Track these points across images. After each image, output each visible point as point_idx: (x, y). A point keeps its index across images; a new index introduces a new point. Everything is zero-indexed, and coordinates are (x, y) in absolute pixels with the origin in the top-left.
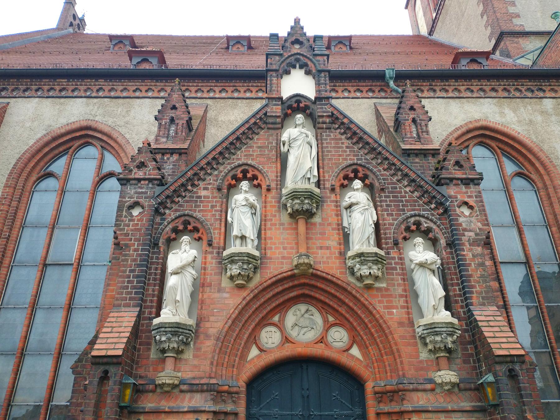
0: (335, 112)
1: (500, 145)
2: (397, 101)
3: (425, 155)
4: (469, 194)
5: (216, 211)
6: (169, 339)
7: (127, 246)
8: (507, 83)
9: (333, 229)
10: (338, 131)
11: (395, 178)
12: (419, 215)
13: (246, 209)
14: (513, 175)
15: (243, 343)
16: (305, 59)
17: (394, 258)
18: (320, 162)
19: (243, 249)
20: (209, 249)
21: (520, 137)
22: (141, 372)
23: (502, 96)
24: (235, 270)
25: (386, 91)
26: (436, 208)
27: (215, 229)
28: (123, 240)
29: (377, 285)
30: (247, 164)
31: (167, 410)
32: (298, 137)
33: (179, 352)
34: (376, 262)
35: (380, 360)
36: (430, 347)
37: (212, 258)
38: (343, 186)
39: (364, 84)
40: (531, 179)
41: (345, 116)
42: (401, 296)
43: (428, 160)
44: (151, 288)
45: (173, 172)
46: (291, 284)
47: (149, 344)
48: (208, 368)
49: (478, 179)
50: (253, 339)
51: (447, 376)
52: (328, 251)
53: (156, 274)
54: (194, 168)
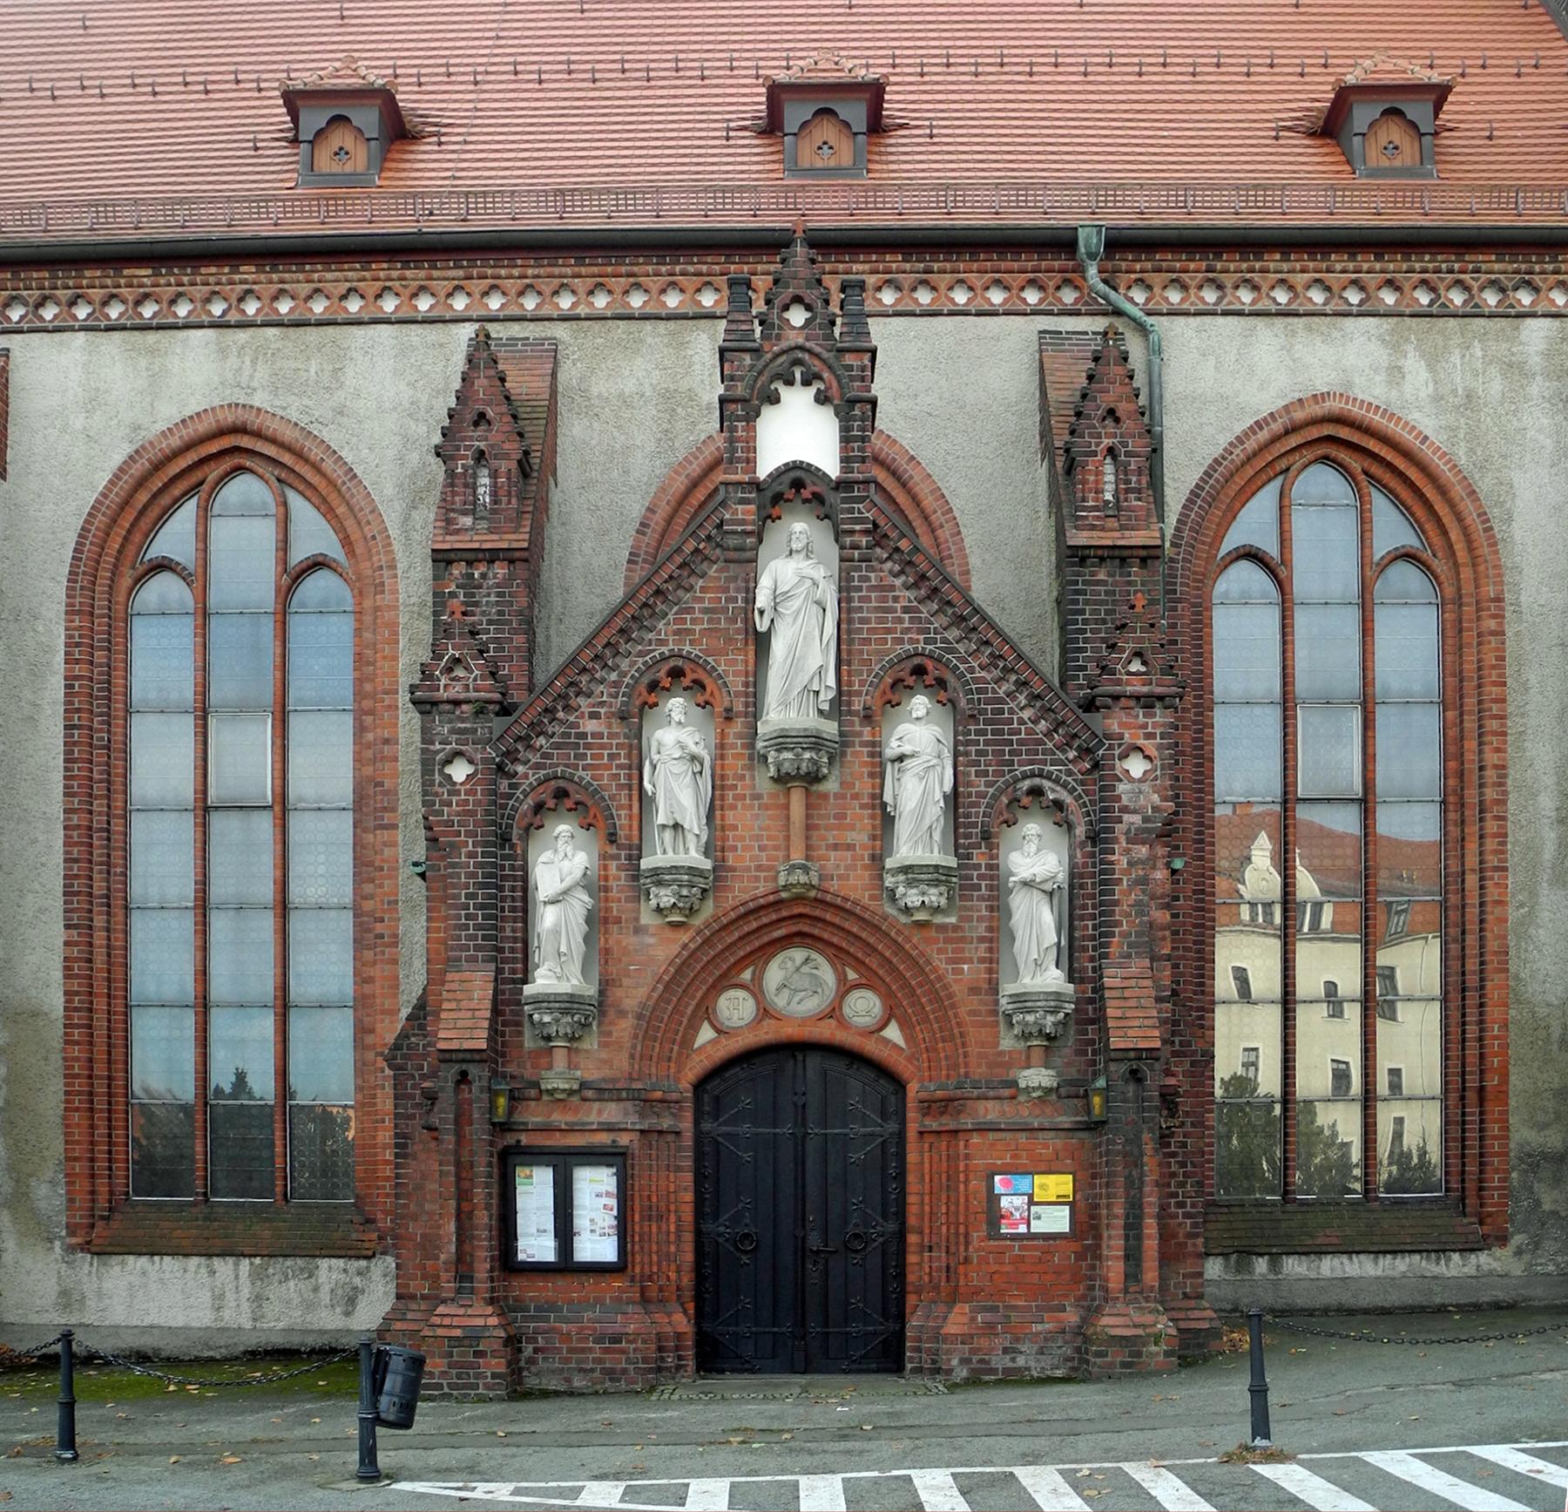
0: (881, 522)
5: (619, 767)
6: (557, 1020)
7: (452, 845)
8: (1431, 266)
9: (862, 807)
10: (889, 564)
12: (1040, 776)
13: (683, 767)
15: (685, 1021)
16: (817, 362)
17: (977, 867)
18: (843, 647)
19: (681, 859)
20: (613, 850)
21: (1426, 452)
22: (511, 1069)
24: (665, 897)
27: (619, 807)
28: (445, 834)
29: (939, 919)
32: (796, 575)
34: (936, 883)
37: (618, 868)
39: (1016, 265)
44: (508, 926)
45: (500, 613)
46: (774, 917)
47: (519, 1024)
48: (625, 1066)
50: (706, 1011)
51: (1037, 1077)
52: (849, 854)
53: (513, 899)
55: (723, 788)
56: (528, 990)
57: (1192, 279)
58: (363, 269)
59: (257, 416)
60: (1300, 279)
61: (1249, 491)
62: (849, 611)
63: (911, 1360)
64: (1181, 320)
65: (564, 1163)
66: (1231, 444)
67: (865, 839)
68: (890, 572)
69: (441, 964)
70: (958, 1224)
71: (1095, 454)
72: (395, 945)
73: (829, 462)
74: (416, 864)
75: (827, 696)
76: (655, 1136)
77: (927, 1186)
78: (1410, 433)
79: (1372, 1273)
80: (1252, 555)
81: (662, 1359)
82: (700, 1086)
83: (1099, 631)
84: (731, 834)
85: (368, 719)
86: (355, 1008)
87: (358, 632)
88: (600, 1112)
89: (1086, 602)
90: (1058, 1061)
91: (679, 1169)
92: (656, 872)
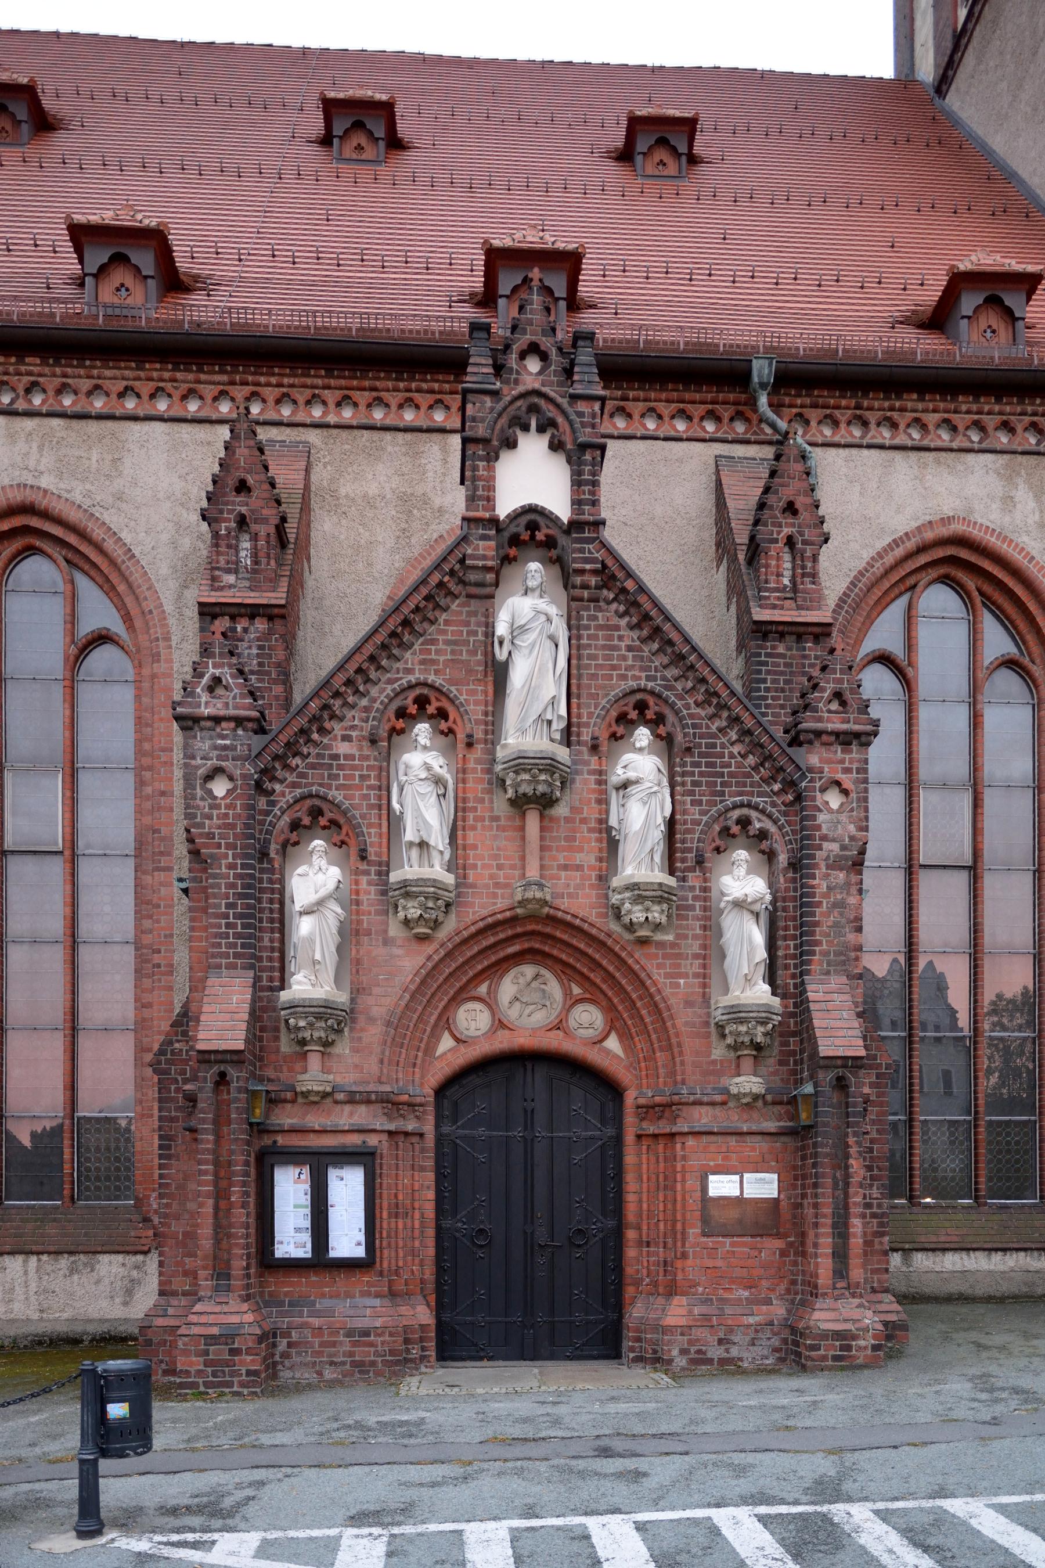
0: (609, 562)
1: (988, 589)
2: (769, 452)
3: (799, 637)
4: (847, 765)
5: (369, 787)
6: (311, 1025)
9: (590, 830)
10: (615, 606)
11: (716, 724)
12: (749, 806)
13: (427, 788)
14: (996, 663)
15: (429, 1029)
16: (551, 407)
17: (692, 888)
18: (574, 681)
19: (426, 872)
20: (364, 866)
22: (270, 1073)
23: (1020, 449)
25: (748, 420)
26: (783, 791)
27: (370, 825)
28: (206, 846)
29: (659, 937)
30: (425, 684)
31: (317, 1128)
32: (529, 612)
33: (327, 1044)
34: (659, 900)
35: (650, 1058)
36: (730, 1040)
37: (369, 883)
38: (614, 737)
39: (698, 396)
40: (1031, 677)
41: (630, 575)
42: (696, 956)
43: (804, 649)
44: (266, 936)
46: (510, 932)
47: (277, 1029)
49: (868, 734)
50: (445, 1022)
51: (748, 1083)
53: (271, 911)
54: (322, 693)
55: (464, 810)
56: (284, 996)
57: (843, 415)
58: (138, 369)
59: (45, 496)
60: (931, 419)
61: (884, 602)
62: (579, 647)
63: (632, 1349)
64: (833, 451)
65: (319, 1164)
66: (873, 558)
67: (593, 862)
68: (616, 612)
69: (203, 968)
70: (666, 1187)
71: (776, 541)
72: (171, 973)
73: (561, 508)
74: (180, 880)
75: (559, 725)
76: (402, 1138)
77: (645, 1185)
78: (1019, 553)
79: (986, 1267)
80: (884, 659)
81: (408, 1351)
82: (440, 1092)
83: (777, 698)
84: (471, 853)
85: (147, 775)
86: (135, 1030)
87: (138, 697)
88: (351, 1114)
89: (768, 672)
90: (763, 1070)
91: (422, 1169)
92: (405, 884)
